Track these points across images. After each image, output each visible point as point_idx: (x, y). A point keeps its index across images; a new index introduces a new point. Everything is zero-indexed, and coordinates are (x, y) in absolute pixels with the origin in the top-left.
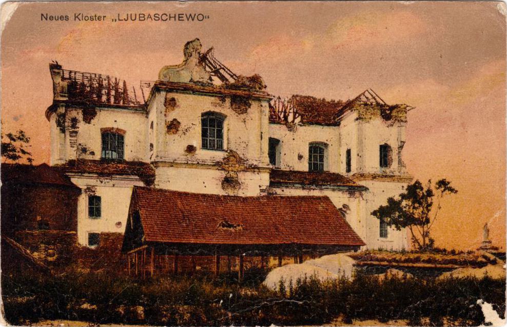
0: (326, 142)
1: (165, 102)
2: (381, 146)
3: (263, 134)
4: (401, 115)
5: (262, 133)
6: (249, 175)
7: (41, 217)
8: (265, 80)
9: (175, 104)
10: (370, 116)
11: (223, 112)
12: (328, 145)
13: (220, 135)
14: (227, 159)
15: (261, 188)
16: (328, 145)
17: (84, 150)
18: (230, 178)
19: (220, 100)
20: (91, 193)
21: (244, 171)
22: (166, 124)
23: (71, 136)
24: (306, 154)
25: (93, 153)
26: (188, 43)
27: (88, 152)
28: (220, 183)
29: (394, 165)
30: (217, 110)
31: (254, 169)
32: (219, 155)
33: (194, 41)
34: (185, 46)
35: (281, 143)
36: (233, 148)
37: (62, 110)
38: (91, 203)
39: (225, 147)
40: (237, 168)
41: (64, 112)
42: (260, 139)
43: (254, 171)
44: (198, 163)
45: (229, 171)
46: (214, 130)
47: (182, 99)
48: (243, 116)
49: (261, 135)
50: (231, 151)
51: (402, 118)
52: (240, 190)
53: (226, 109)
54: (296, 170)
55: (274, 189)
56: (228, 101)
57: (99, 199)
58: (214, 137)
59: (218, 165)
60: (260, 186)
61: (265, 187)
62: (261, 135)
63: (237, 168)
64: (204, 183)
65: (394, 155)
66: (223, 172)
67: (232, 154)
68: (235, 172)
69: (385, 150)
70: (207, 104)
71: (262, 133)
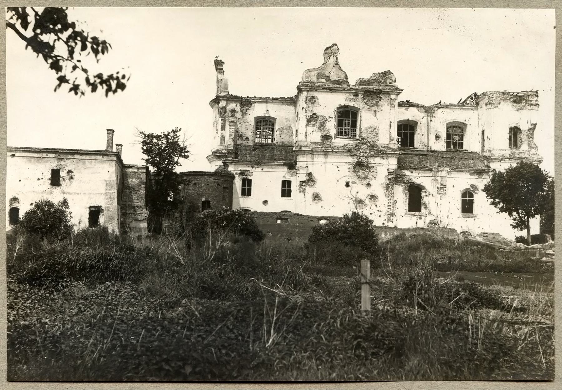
0: (464, 122)
1: (306, 100)
2: (511, 129)
3: (392, 124)
4: (532, 99)
5: (391, 122)
6: (378, 160)
7: (492, 359)
8: (396, 75)
9: (315, 101)
10: (499, 101)
11: (356, 106)
12: (467, 125)
13: (354, 125)
14: (358, 147)
15: (389, 171)
16: (467, 125)
17: (241, 136)
18: (361, 162)
19: (354, 96)
20: (244, 177)
21: (373, 156)
22: (306, 118)
23: (230, 126)
24: (444, 135)
25: (247, 139)
26: (327, 49)
27: (244, 138)
28: (352, 167)
29: (524, 147)
30: (351, 104)
31: (381, 153)
32: (350, 143)
33: (332, 46)
34: (325, 50)
35: (419, 124)
36: (364, 135)
37: (223, 103)
38: (244, 184)
39: (357, 137)
40: (367, 154)
41: (224, 105)
42: (389, 128)
43: (383, 157)
44: (333, 151)
45: (360, 157)
46: (342, 129)
47: (321, 97)
48: (374, 108)
49: (390, 124)
50: (363, 139)
51: (533, 102)
52: (370, 173)
53: (359, 104)
54: (433, 150)
55: (404, 171)
56: (360, 96)
57: (250, 181)
58: (349, 126)
59: (349, 151)
60: (388, 170)
61: (393, 170)
62: (390, 124)
63: (367, 154)
64: (338, 167)
65: (523, 137)
66: (355, 157)
67: (363, 140)
68: (366, 157)
69: (515, 132)
70: (341, 99)
71: (391, 122)
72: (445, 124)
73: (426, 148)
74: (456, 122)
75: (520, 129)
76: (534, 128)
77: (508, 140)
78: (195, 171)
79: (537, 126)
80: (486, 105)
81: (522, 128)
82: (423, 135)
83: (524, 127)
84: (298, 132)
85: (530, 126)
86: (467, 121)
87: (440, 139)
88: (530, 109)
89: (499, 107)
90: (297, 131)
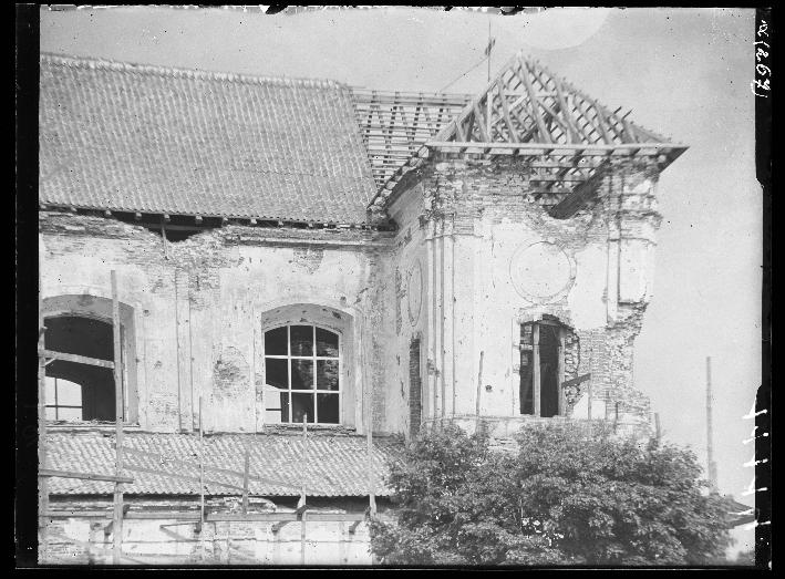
0: (337, 306)
72: (258, 314)
73: (175, 420)
74: (305, 308)
75: (568, 330)
76: (633, 323)
77: (517, 378)
78: (212, 11)
79: (646, 315)
80: (423, 222)
81: (578, 324)
82: (159, 364)
83: (586, 315)
84: (712, 361)
85: (616, 314)
86: (349, 302)
87: (238, 384)
88: (615, 234)
89: (477, 231)
90: (656, 415)
